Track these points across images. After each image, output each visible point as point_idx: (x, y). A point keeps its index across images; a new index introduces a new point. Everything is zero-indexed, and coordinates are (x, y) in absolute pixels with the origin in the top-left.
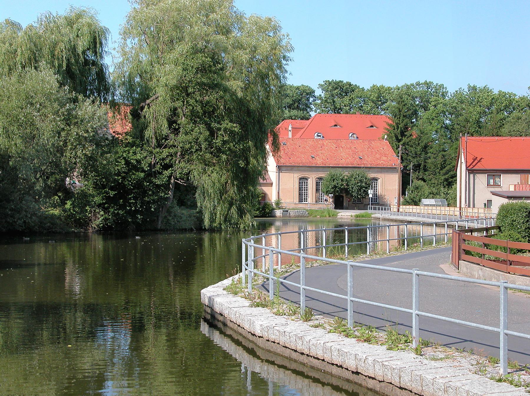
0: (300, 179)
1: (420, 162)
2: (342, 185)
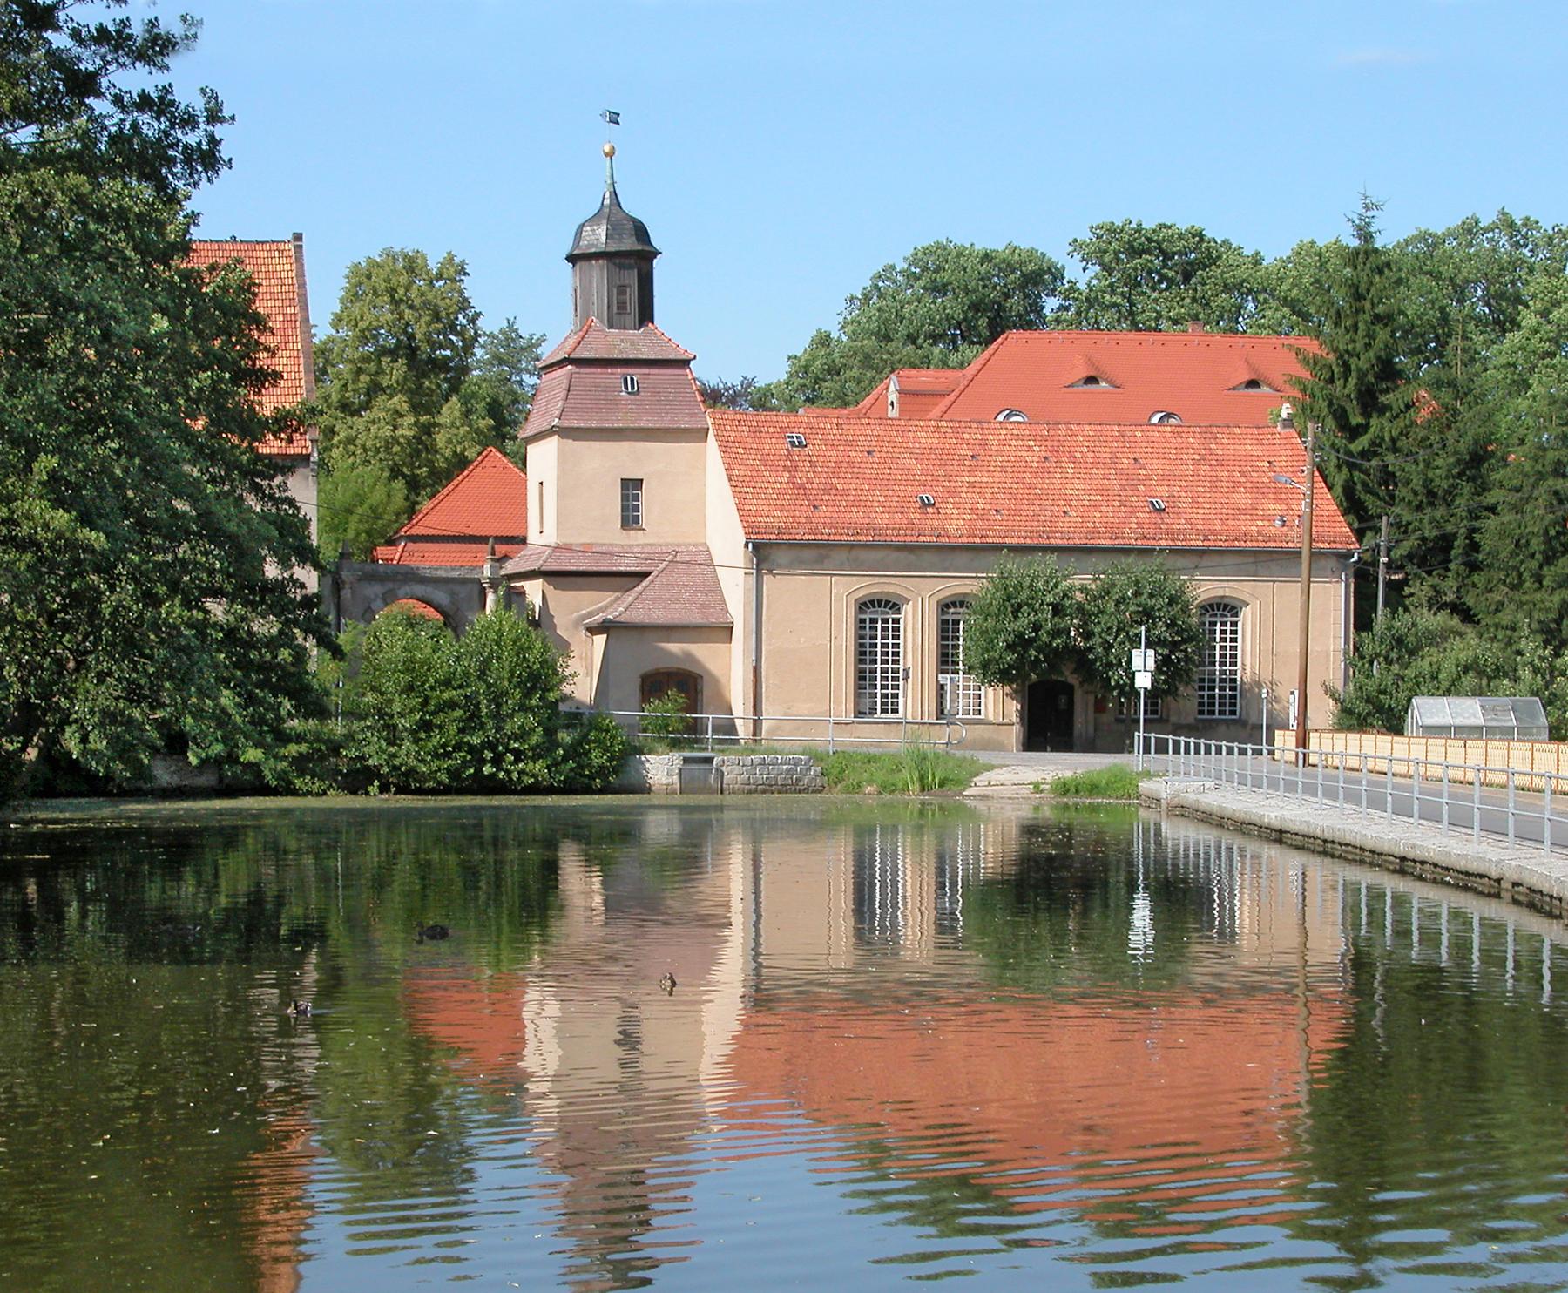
0: (944, 606)
1: (1449, 528)
2: (1056, 633)
